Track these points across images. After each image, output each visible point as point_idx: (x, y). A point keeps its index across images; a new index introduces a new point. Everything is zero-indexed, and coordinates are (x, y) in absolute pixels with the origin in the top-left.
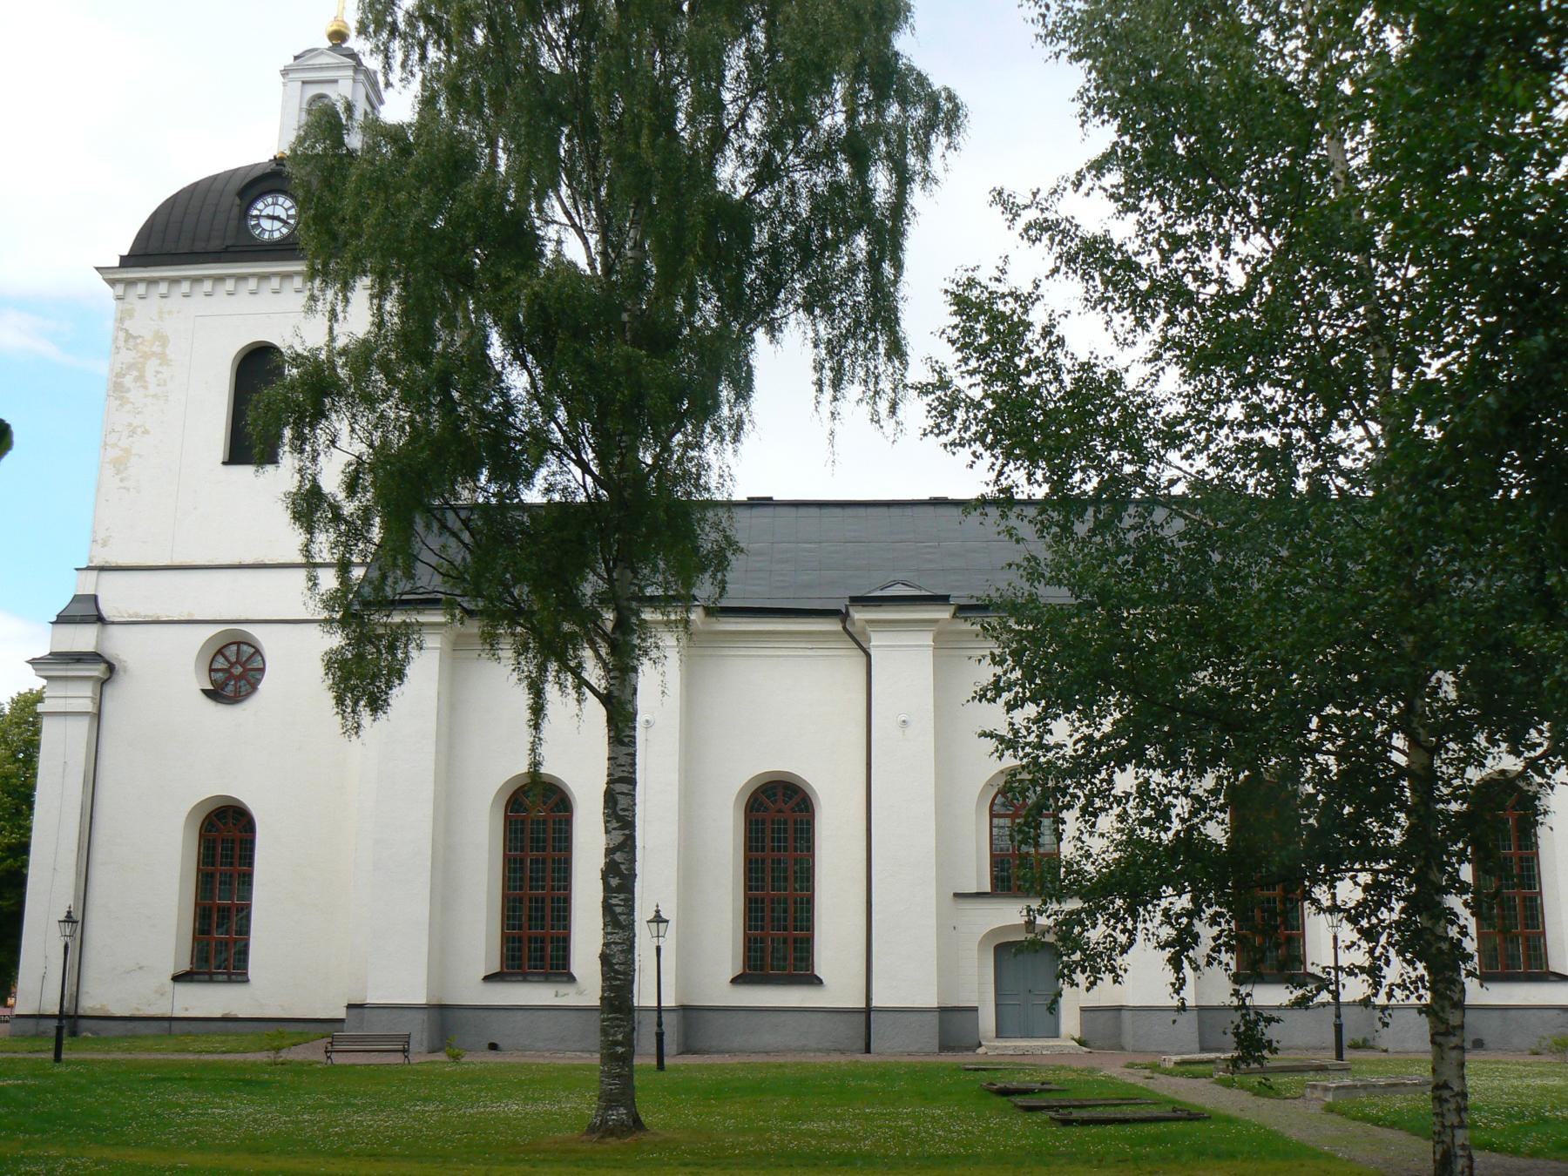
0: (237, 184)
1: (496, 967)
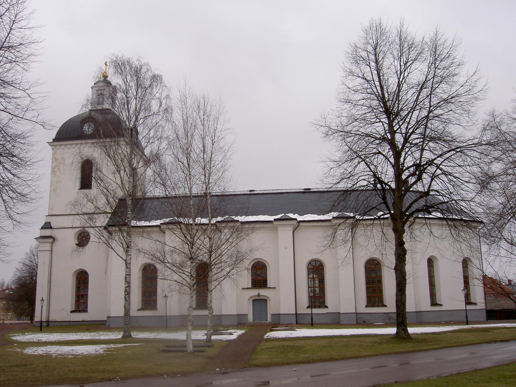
0: (80, 119)
1: (140, 307)
